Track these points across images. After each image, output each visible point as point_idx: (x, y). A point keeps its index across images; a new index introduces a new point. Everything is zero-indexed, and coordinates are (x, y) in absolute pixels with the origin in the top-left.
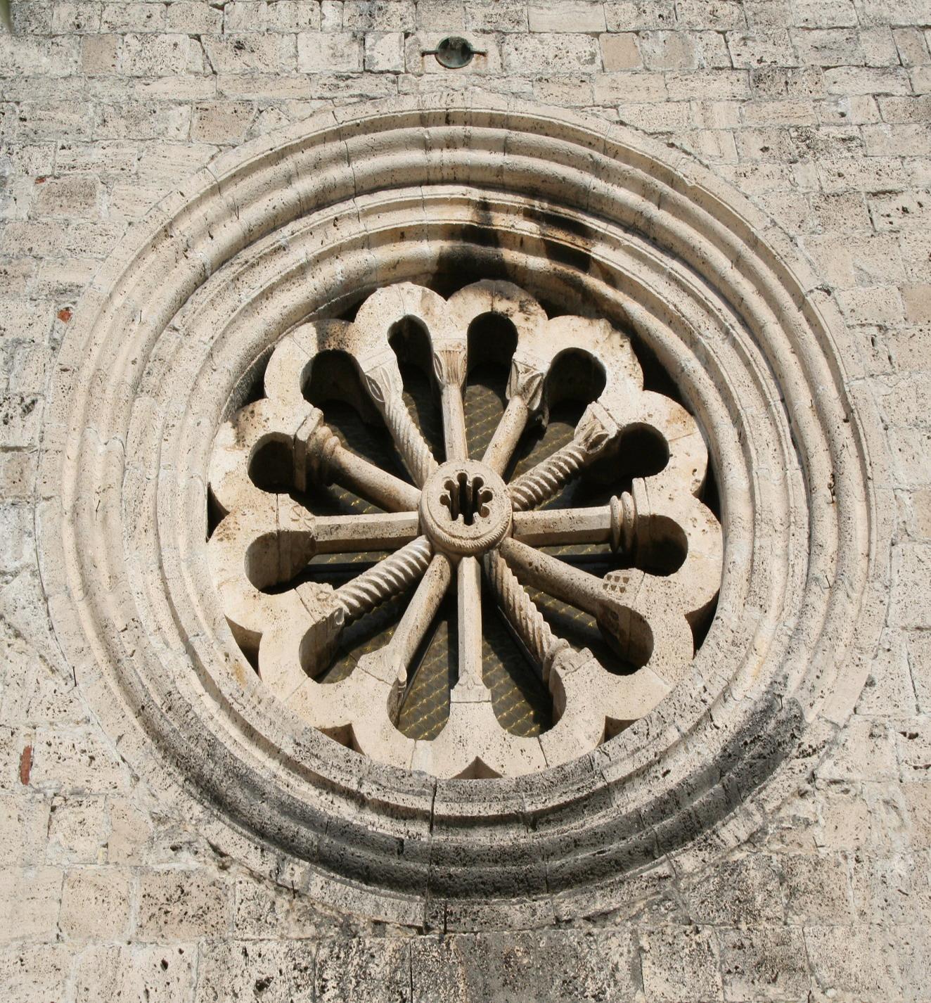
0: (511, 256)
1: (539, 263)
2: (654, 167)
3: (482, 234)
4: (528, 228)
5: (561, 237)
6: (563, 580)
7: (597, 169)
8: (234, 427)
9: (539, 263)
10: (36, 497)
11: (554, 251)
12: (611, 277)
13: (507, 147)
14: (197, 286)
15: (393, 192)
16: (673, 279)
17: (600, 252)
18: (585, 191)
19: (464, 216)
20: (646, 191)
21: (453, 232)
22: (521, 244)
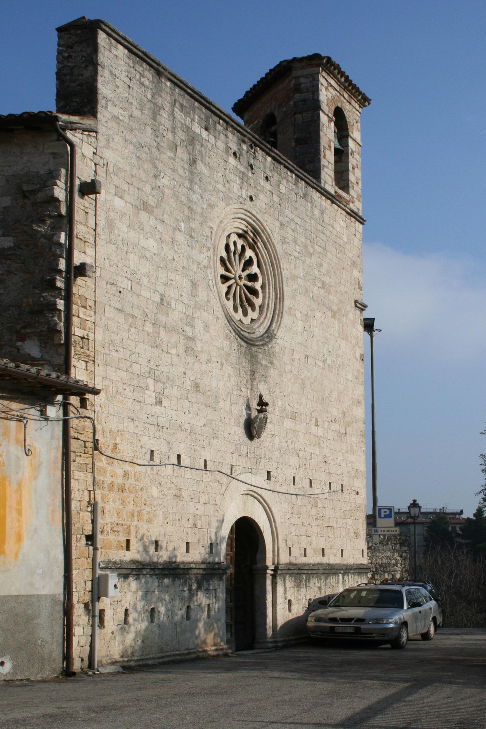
0: (249, 238)
1: (251, 240)
2: (269, 235)
3: (246, 232)
4: (251, 234)
5: (255, 238)
6: (72, 631)
7: (263, 231)
8: (97, 440)
9: (251, 240)
10: (139, 143)
11: (253, 239)
12: (258, 247)
13: (254, 221)
14: (147, 666)
15: (271, 599)
16: (265, 253)
17: (259, 244)
18: (260, 234)
19: (245, 229)
20: (267, 239)
21: (243, 230)
22: (250, 236)
